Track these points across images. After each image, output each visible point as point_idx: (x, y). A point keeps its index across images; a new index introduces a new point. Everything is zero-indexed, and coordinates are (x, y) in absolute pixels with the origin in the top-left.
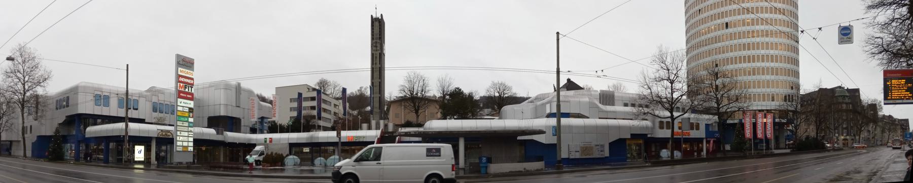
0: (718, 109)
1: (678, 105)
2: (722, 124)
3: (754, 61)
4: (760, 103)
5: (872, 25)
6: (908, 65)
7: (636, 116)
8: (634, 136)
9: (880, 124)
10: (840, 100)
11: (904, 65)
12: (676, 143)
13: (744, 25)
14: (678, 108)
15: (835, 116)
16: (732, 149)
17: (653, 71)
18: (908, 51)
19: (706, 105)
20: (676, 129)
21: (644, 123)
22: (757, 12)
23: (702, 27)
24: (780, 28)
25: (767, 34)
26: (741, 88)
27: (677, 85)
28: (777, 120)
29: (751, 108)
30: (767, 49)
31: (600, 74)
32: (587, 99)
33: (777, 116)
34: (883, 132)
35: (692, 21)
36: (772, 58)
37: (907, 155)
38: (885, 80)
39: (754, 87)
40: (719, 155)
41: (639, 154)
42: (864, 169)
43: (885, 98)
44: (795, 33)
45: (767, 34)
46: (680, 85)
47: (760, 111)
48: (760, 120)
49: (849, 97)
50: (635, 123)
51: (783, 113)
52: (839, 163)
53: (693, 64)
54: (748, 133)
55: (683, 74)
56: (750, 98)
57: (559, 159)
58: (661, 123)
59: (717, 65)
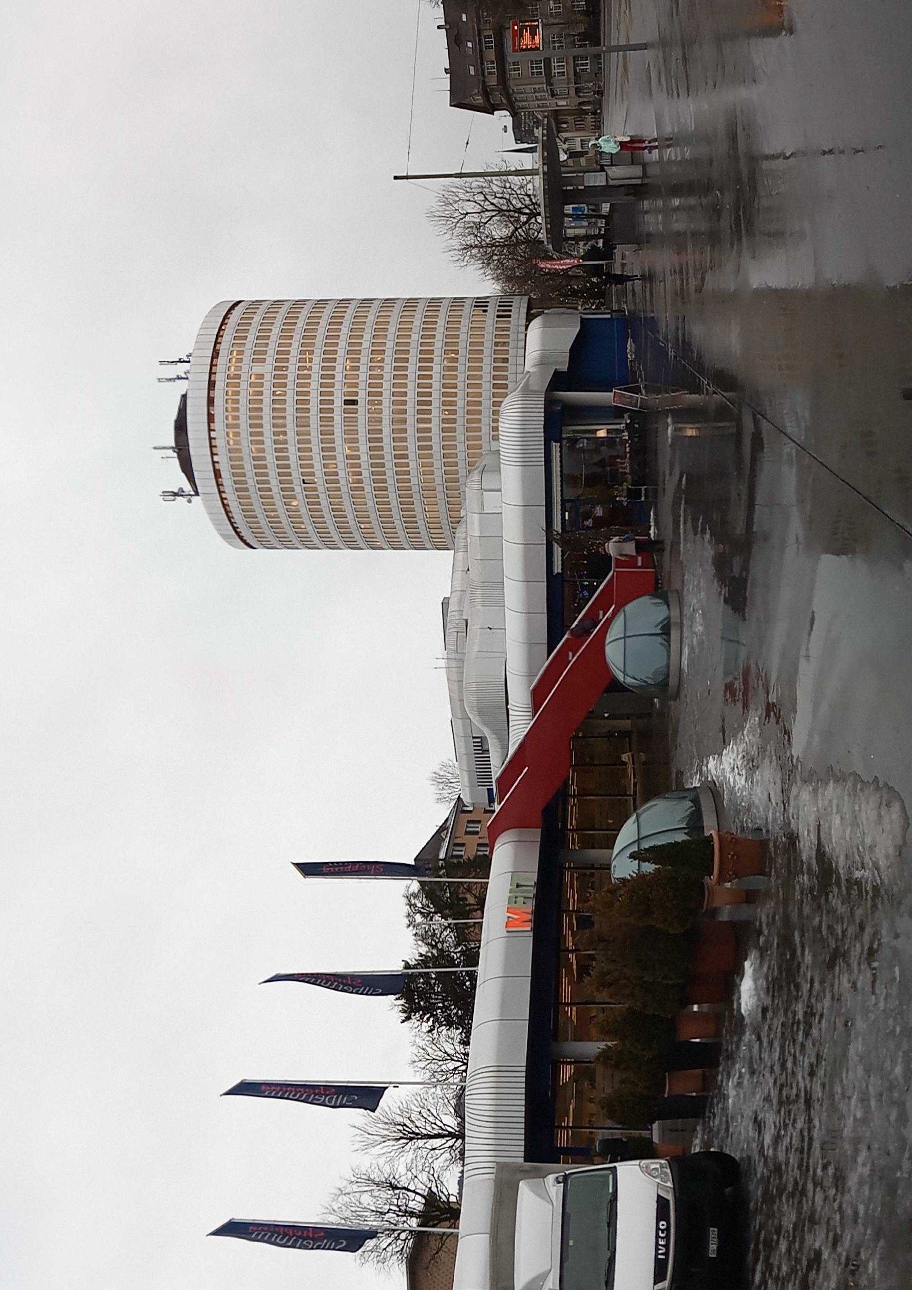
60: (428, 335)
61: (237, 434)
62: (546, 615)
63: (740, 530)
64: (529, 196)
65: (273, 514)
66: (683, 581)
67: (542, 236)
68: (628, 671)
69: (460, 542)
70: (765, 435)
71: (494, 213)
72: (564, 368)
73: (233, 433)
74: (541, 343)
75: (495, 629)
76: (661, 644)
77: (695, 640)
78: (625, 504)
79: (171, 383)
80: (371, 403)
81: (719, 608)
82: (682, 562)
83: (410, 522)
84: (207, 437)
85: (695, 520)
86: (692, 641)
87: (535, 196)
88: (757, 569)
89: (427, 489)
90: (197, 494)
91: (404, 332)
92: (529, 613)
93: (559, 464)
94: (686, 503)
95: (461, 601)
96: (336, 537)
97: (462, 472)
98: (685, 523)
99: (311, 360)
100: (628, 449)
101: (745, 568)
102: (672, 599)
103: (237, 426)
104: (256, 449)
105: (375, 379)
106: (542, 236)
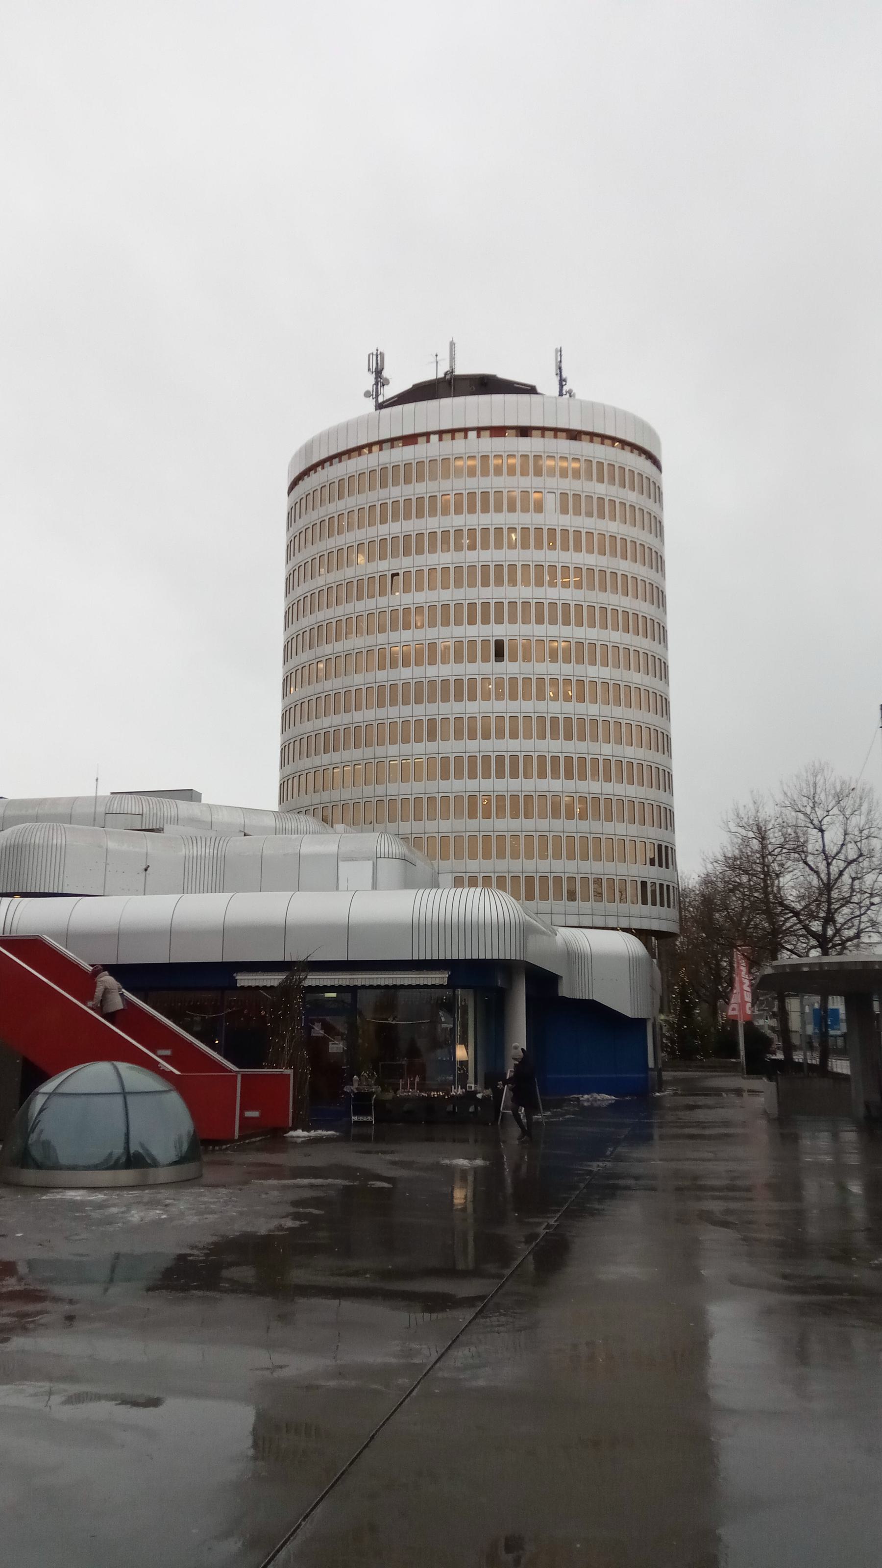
60: (608, 769)
61: (472, 472)
62: (166, 961)
63: (299, 1276)
64: (857, 936)
65: (345, 524)
66: (217, 1186)
67: (785, 958)
68: (55, 1100)
69: (292, 822)
70: (449, 1314)
71: (823, 876)
72: (565, 990)
73: (475, 467)
74: (603, 954)
75: (146, 876)
76: (111, 1154)
77: (114, 1210)
78: (347, 1089)
79: (553, 369)
80: (499, 682)
81: (169, 1247)
82: (246, 1183)
83: (330, 741)
84: (468, 425)
85: (317, 1202)
86: (114, 1205)
87: (857, 946)
88: (231, 1305)
89: (377, 771)
90: (380, 406)
91: (615, 731)
92: (171, 933)
93: (414, 983)
94: (345, 1187)
95: (193, 821)
96: (307, 621)
97: (405, 827)
98: (312, 1186)
99: (565, 585)
100: (434, 1094)
101: (240, 1288)
102: (190, 1169)
103: (485, 473)
104: (448, 501)
105: (540, 688)
106: (785, 958)
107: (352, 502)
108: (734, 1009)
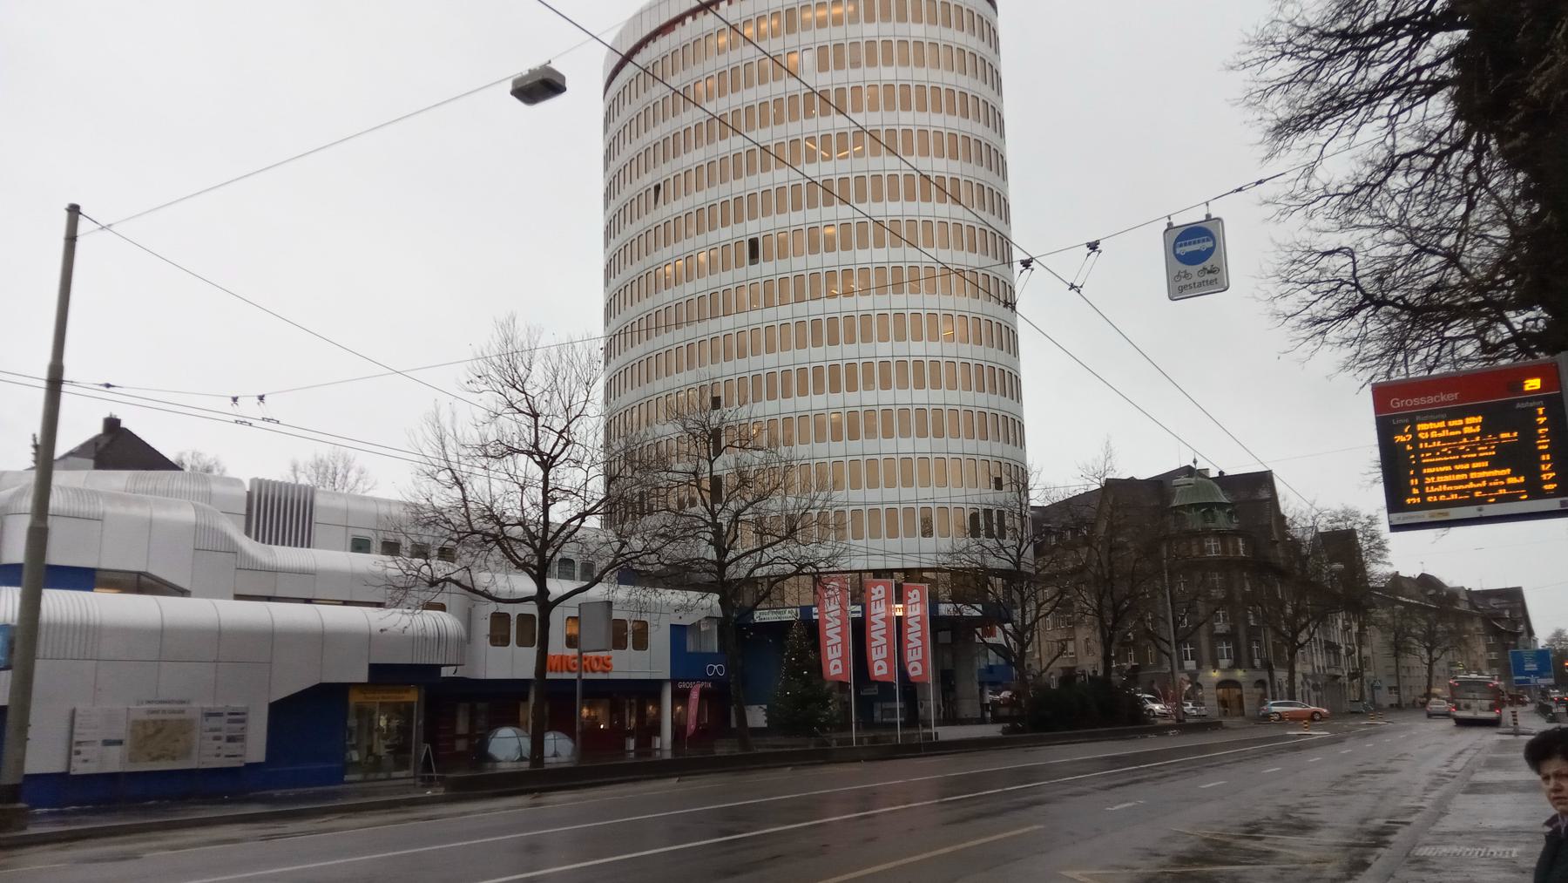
0: (722, 566)
1: (569, 550)
2: (737, 629)
3: (852, 387)
4: (877, 544)
5: (1302, 202)
6: (1485, 347)
7: (396, 594)
8: (383, 675)
9: (1383, 614)
10: (1195, 522)
11: (1469, 349)
12: (552, 701)
13: (814, 249)
14: (567, 562)
15: (1175, 593)
16: (778, 725)
17: (476, 415)
18: (1477, 287)
19: (676, 551)
20: (557, 646)
21: (430, 621)
22: (861, 198)
23: (665, 253)
24: (945, 256)
25: (897, 280)
26: (806, 487)
27: (567, 476)
28: (945, 609)
29: (844, 564)
30: (900, 337)
31: (250, 410)
32: (187, 514)
33: (944, 593)
34: (1399, 648)
35: (630, 231)
36: (920, 373)
37: (1538, 752)
38: (1386, 429)
39: (856, 485)
40: (722, 750)
41: (401, 751)
42: (1323, 814)
43: (1395, 501)
44: (999, 270)
45: (897, 280)
46: (580, 475)
47: (878, 573)
48: (882, 610)
49: (1233, 510)
50: (393, 619)
51: (966, 581)
52: (1211, 783)
53: (629, 397)
54: (836, 661)
55: (590, 431)
56: (839, 527)
57: (9, 779)
58: (500, 620)
59: (716, 402)
107: (695, 157)
108: (880, 668)
